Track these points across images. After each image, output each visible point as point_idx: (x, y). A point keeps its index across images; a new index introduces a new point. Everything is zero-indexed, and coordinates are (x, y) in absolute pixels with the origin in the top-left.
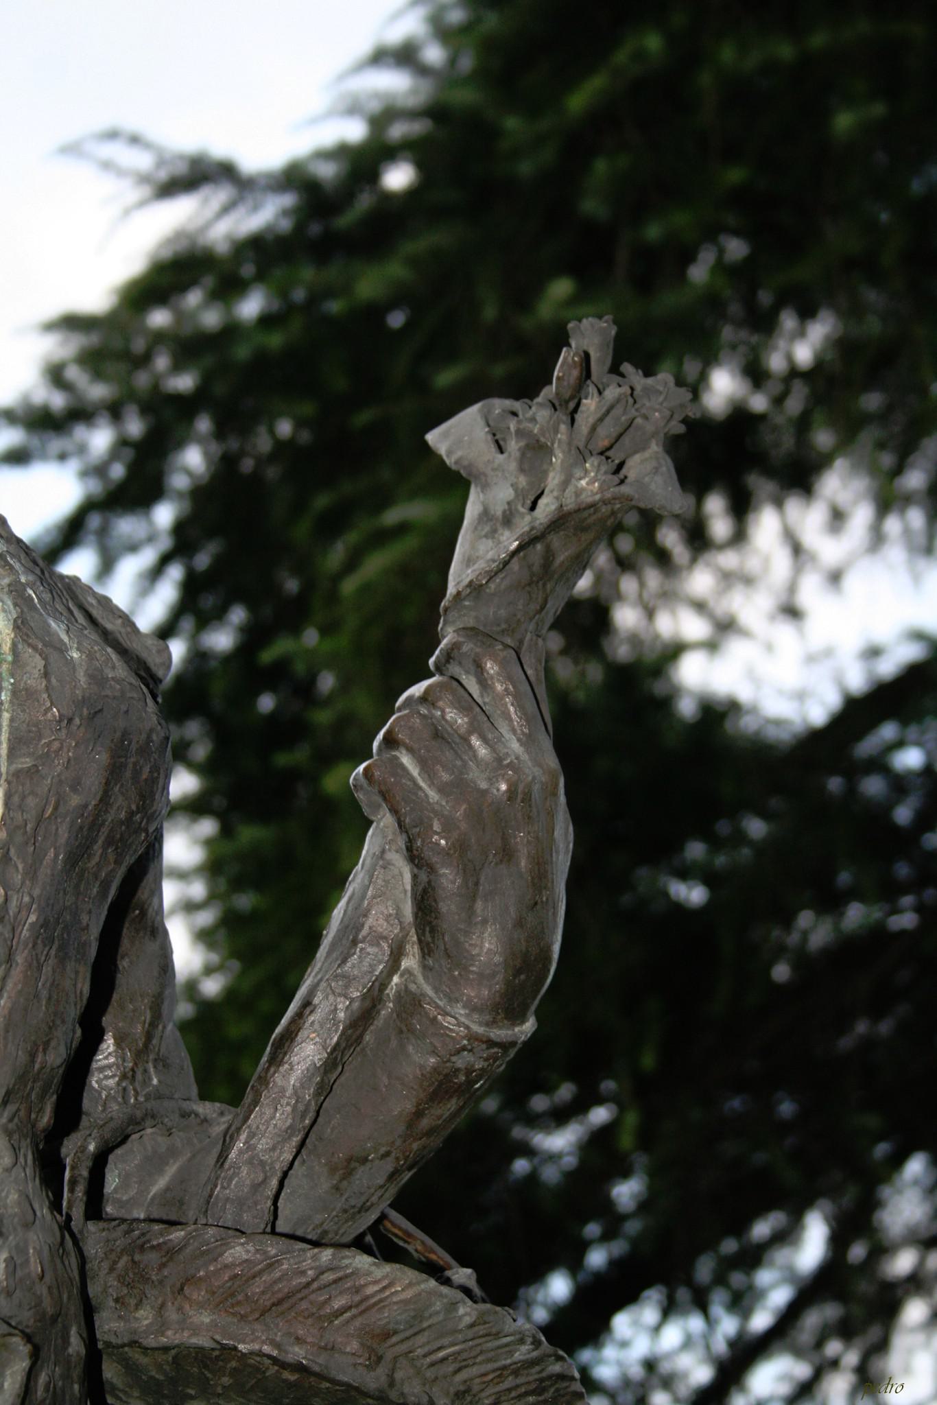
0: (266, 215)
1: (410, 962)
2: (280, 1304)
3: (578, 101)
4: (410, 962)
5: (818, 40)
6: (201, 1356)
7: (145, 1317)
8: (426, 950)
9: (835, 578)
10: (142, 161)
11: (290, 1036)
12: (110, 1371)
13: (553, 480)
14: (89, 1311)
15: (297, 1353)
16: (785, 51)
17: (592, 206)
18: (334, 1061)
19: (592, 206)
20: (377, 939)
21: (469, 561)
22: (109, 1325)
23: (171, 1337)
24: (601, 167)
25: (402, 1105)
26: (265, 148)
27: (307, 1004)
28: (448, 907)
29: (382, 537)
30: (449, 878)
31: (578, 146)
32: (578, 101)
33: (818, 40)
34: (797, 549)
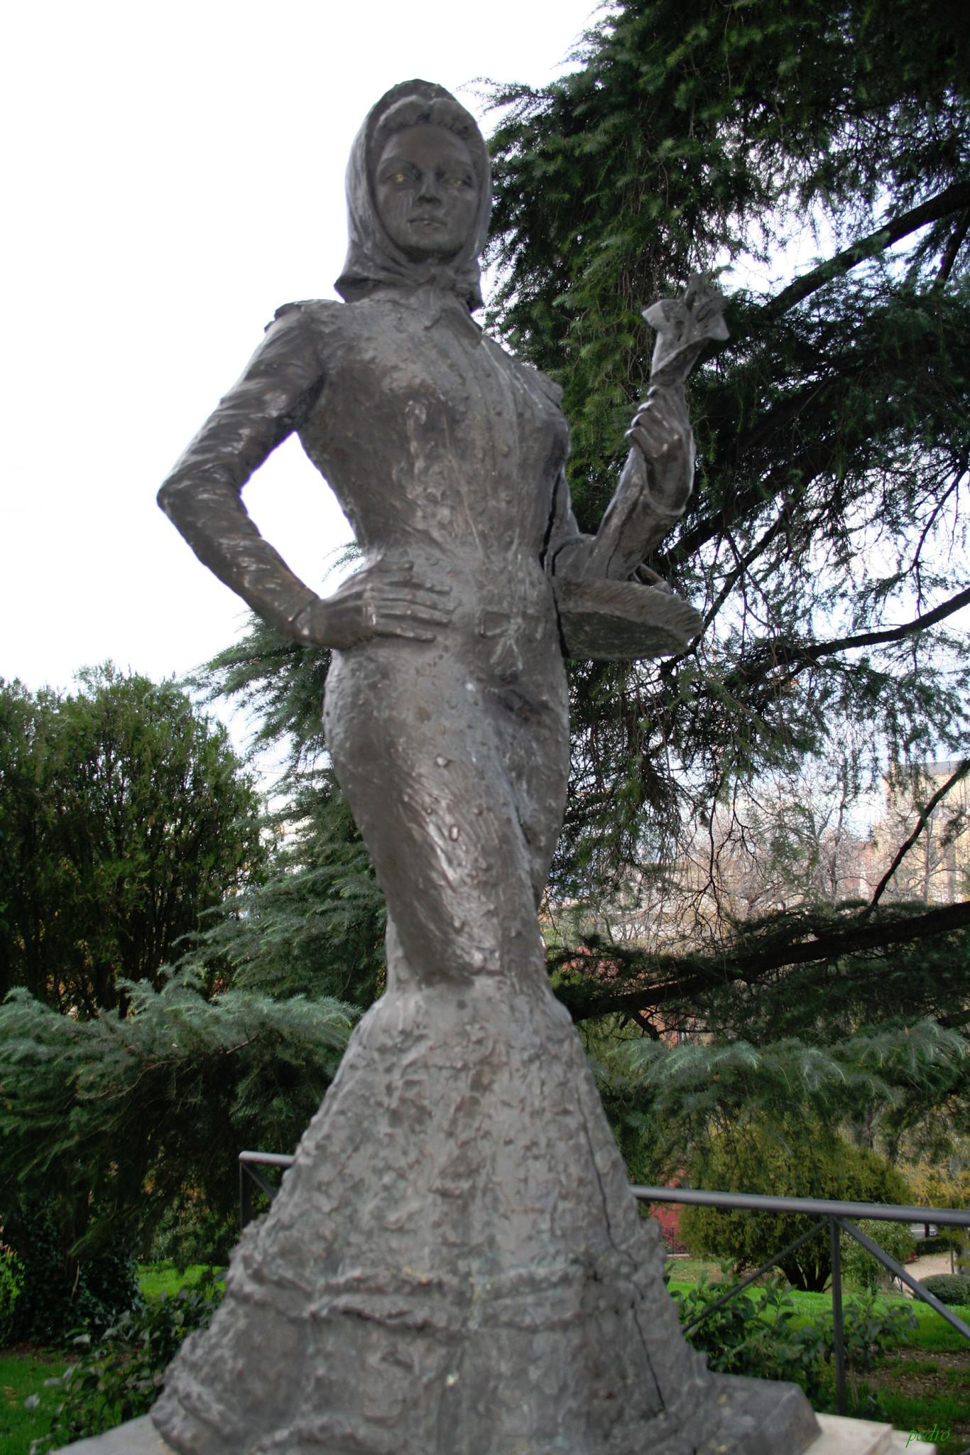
0: (542, 107)
1: (646, 492)
2: (611, 600)
3: (672, 60)
4: (646, 492)
5: (771, 29)
6: (589, 615)
7: (571, 604)
8: (651, 489)
9: (783, 243)
10: (491, 90)
11: (609, 517)
12: (563, 621)
13: (685, 331)
14: (556, 602)
15: (618, 613)
16: (758, 36)
17: (679, 104)
18: (624, 524)
19: (679, 104)
20: (635, 485)
21: (660, 359)
22: (562, 607)
23: (580, 610)
24: (683, 87)
25: (645, 536)
26: (539, 83)
27: (615, 507)
28: (658, 476)
29: (598, 251)
30: (658, 468)
31: (675, 78)
32: (672, 60)
33: (771, 29)
34: (766, 232)
